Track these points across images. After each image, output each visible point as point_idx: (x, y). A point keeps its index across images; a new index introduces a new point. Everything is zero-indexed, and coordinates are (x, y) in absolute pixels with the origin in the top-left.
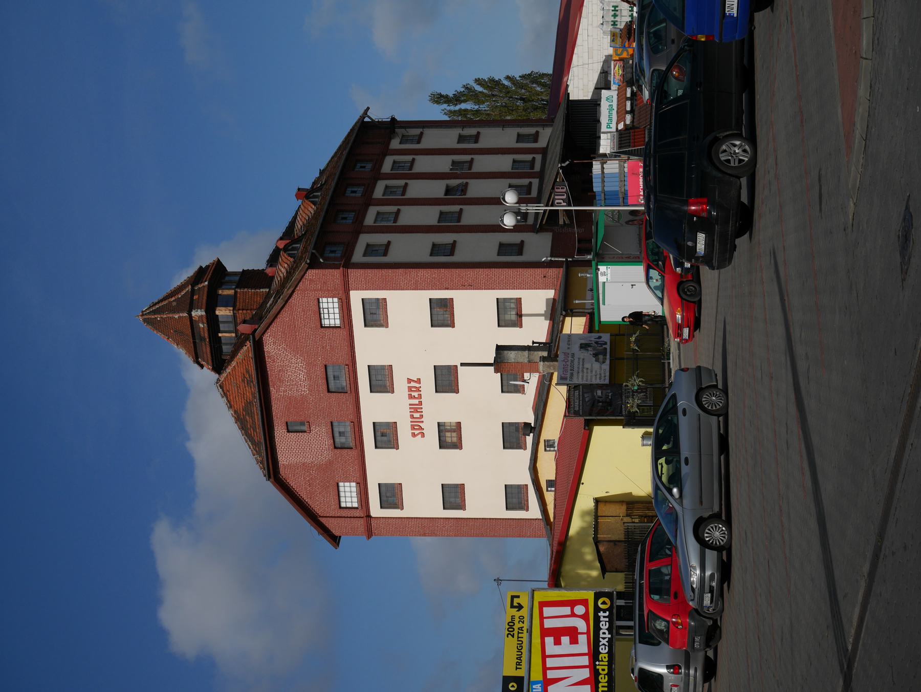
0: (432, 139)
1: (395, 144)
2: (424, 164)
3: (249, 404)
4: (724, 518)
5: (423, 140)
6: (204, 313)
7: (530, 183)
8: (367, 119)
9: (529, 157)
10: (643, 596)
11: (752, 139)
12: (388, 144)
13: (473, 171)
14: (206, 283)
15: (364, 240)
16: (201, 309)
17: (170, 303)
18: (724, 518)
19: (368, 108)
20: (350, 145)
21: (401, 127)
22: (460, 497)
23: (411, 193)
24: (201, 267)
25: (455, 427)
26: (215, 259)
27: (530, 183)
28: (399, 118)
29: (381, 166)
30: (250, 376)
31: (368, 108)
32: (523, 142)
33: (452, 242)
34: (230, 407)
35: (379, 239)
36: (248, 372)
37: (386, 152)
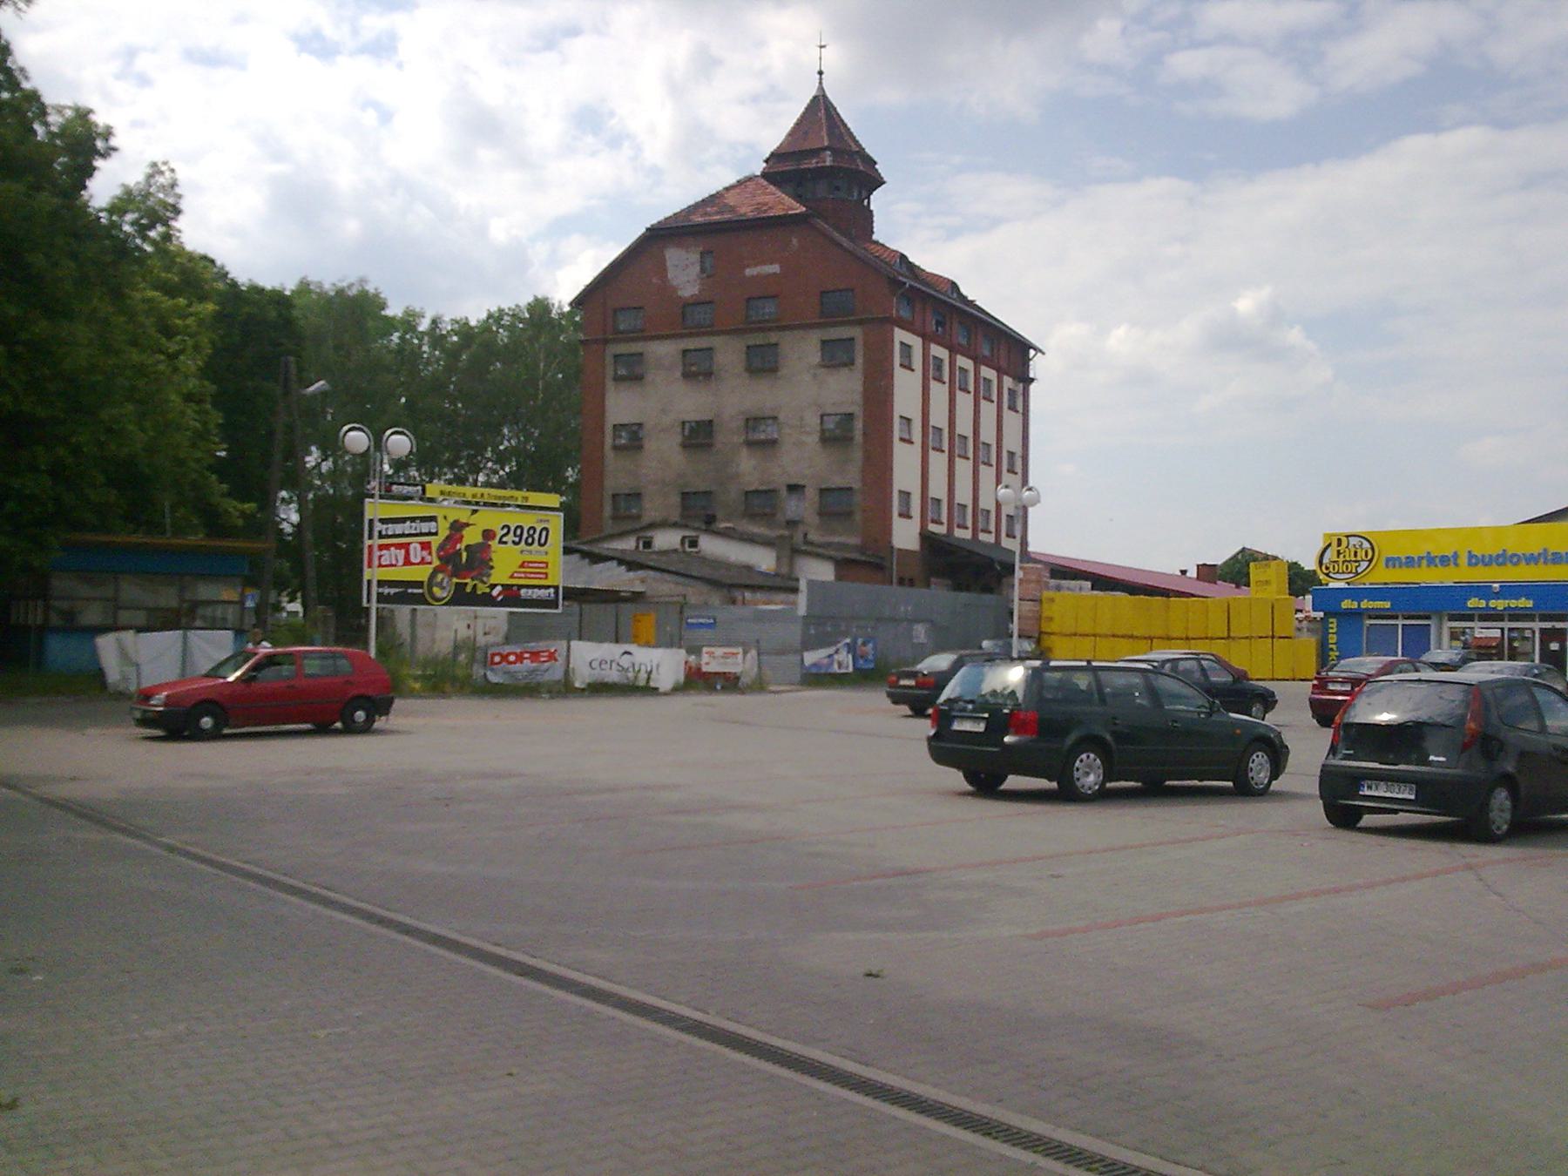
0: (1012, 420)
1: (1008, 382)
2: (988, 410)
3: (732, 209)
4: (1109, 785)
5: (962, 393)
6: (828, 164)
7: (942, 523)
8: (1032, 352)
9: (992, 528)
10: (1387, 803)
11: (1103, 796)
12: (1007, 374)
13: (957, 459)
14: (861, 168)
15: (916, 342)
16: (834, 161)
17: (839, 127)
18: (1109, 785)
19: (1043, 353)
20: (924, 289)
21: (1024, 388)
22: (1191, 614)
23: (960, 396)
24: (875, 163)
25: (501, 343)
26: (885, 179)
27: (942, 523)
28: (1033, 387)
29: (939, 344)
30: (765, 211)
31: (1043, 353)
32: (1007, 521)
33: (914, 440)
34: (727, 189)
35: (917, 362)
36: (770, 208)
37: (1001, 372)
